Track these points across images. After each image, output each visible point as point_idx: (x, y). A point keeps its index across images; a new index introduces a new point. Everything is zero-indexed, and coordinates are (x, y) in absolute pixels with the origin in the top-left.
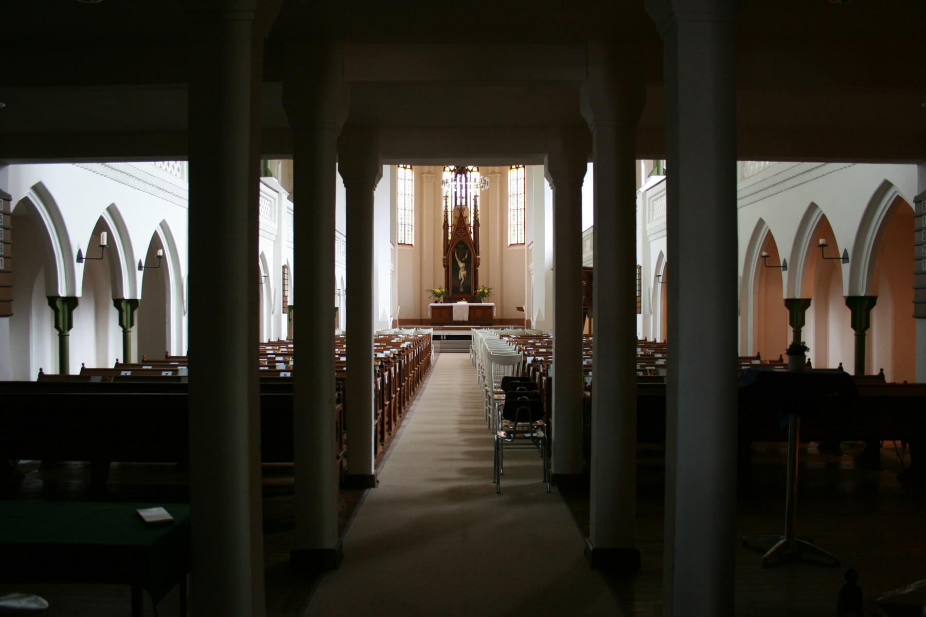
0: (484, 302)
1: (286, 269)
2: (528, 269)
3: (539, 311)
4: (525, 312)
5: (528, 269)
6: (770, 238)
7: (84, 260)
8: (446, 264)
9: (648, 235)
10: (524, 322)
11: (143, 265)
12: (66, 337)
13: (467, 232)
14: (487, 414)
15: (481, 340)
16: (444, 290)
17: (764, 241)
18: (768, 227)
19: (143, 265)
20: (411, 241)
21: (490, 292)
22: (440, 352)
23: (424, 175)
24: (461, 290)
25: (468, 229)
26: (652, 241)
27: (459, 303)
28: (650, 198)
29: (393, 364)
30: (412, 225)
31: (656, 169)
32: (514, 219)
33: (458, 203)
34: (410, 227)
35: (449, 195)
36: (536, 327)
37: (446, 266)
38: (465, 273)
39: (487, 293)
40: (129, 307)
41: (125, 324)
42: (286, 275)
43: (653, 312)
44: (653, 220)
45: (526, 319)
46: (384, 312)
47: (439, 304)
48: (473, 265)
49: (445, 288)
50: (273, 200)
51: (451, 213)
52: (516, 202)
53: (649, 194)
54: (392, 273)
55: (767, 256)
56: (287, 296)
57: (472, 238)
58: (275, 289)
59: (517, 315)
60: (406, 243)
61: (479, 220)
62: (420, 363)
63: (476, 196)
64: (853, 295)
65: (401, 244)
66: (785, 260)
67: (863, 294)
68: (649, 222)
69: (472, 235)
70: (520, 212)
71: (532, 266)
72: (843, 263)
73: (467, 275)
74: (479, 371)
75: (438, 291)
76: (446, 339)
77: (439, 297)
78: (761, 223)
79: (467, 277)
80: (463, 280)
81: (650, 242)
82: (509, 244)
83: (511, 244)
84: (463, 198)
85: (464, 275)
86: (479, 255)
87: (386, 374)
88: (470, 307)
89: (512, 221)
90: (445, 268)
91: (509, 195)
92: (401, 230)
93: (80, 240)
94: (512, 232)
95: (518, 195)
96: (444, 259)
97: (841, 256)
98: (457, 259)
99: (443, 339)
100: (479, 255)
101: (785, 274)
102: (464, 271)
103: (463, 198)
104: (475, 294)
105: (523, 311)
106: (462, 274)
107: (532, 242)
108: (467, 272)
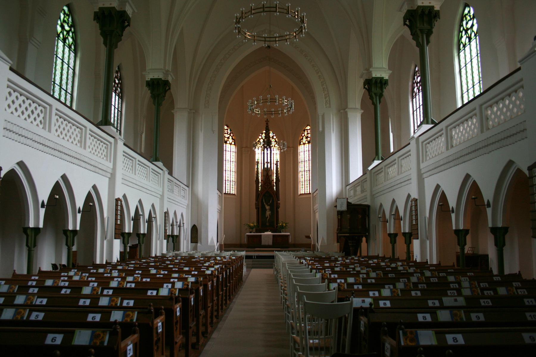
0: (283, 232)
1: (166, 214)
2: (313, 209)
3: (323, 238)
4: (312, 239)
5: (313, 209)
6: (443, 195)
7: (81, 212)
8: (257, 207)
9: (422, 172)
10: (311, 246)
11: (81, 210)
12: (71, 250)
13: (271, 185)
14: (286, 320)
15: (284, 265)
16: (255, 224)
17: (511, 182)
18: (442, 189)
19: (81, 210)
21: (287, 226)
22: (252, 268)
23: (244, 149)
24: (267, 224)
26: (425, 178)
27: (266, 233)
28: (423, 142)
29: (225, 270)
30: (235, 182)
31: (377, 156)
32: (302, 178)
33: (266, 166)
34: (234, 182)
35: (260, 161)
36: (320, 250)
37: (257, 208)
39: (285, 226)
40: (72, 235)
41: (69, 244)
42: (166, 217)
43: (429, 237)
44: (426, 160)
45: (312, 243)
46: (212, 239)
47: (252, 234)
48: (275, 208)
49: (257, 223)
50: (109, 144)
51: (260, 174)
52: (303, 166)
53: (422, 139)
54: (219, 212)
55: (476, 198)
56: (167, 230)
57: (275, 189)
58: (108, 218)
59: (305, 241)
60: (231, 193)
61: (279, 178)
62: (239, 274)
63: (277, 162)
64: (457, 229)
65: (228, 194)
66: (488, 200)
67: (500, 226)
68: (423, 162)
69: (275, 187)
70: (307, 173)
71: (317, 206)
72: (487, 207)
73: (271, 214)
74: (282, 286)
75: (252, 225)
76: (256, 258)
77: (252, 229)
78: (438, 187)
79: (272, 215)
81: (424, 179)
82: (299, 193)
83: (301, 194)
84: (269, 163)
85: (269, 214)
87: (228, 271)
88: (273, 236)
89: (301, 179)
90: (256, 209)
91: (299, 161)
92: (228, 185)
93: (44, 195)
95: (305, 162)
96: (256, 203)
97: (486, 204)
98: (265, 204)
99: (254, 258)
100: (279, 201)
102: (269, 211)
103: (269, 163)
104: (277, 227)
105: (310, 238)
106: (268, 213)
107: (317, 190)
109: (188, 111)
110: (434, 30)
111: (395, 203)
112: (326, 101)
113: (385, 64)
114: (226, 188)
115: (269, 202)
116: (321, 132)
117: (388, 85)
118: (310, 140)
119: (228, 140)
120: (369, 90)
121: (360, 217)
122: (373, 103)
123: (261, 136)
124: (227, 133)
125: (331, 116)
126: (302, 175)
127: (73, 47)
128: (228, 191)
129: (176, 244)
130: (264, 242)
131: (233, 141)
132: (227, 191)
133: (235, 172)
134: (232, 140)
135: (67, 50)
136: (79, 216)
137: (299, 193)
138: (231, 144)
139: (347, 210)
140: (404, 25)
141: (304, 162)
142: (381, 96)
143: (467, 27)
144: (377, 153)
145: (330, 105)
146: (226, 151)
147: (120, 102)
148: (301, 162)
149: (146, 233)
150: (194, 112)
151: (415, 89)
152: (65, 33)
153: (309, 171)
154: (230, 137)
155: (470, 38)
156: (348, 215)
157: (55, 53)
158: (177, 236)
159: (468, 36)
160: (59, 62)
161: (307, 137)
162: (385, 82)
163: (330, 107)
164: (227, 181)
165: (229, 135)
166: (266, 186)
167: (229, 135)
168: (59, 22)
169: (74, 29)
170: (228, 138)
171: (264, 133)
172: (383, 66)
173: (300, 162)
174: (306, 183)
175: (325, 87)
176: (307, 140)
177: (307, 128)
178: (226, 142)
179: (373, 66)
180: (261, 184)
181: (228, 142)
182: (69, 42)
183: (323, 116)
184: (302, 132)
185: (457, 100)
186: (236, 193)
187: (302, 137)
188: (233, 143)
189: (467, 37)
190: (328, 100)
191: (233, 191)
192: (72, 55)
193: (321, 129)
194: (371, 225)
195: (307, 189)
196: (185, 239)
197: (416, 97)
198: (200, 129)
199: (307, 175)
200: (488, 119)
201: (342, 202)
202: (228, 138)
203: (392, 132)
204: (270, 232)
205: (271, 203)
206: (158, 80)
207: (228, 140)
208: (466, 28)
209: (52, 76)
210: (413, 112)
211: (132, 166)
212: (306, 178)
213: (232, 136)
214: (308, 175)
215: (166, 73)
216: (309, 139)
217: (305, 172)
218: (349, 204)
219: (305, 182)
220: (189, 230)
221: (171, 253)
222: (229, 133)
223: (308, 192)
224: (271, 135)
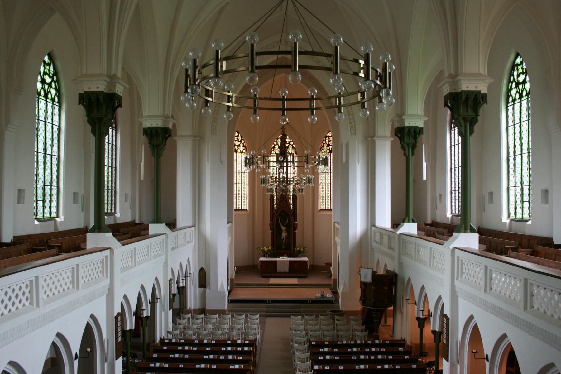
3: (345, 284)
16: (270, 248)
20: (246, 207)
21: (305, 250)
22: (267, 316)
24: (283, 247)
25: (289, 201)
30: (247, 195)
32: (323, 191)
34: (246, 196)
37: (272, 229)
38: (286, 234)
39: (303, 251)
46: (222, 284)
48: (292, 228)
49: (272, 245)
52: (324, 178)
58: (108, 340)
60: (243, 208)
65: (239, 210)
69: (292, 206)
70: (328, 186)
78: (471, 318)
80: (285, 240)
82: (319, 209)
83: (321, 210)
85: (285, 236)
86: (297, 221)
88: (290, 262)
89: (321, 192)
90: (271, 231)
92: (239, 199)
94: (321, 201)
96: (270, 224)
98: (280, 224)
100: (297, 221)
101: (487, 364)
102: (285, 233)
104: (294, 250)
106: (284, 234)
108: (288, 234)
109: (193, 139)
110: (479, 118)
111: (424, 291)
112: (351, 128)
113: (420, 111)
114: (237, 203)
115: (286, 223)
116: (344, 163)
117: (423, 134)
118: (332, 149)
119: (239, 149)
120: (401, 139)
121: (386, 289)
122: (405, 154)
123: (276, 141)
124: (237, 140)
125: (357, 144)
126: (323, 188)
127: (56, 99)
128: (239, 206)
129: (182, 296)
130: (279, 269)
131: (244, 149)
132: (237, 206)
133: (247, 184)
134: (243, 148)
135: (50, 105)
136: (76, 363)
137: (319, 209)
138: (242, 152)
139: (371, 282)
140: (445, 107)
141: (325, 174)
142: (414, 147)
143: (518, 80)
144: (407, 214)
145: (355, 131)
146: (236, 161)
147: (114, 134)
148: (321, 173)
149: (149, 315)
150: (199, 139)
151: (513, 92)
152: (46, 86)
153: (331, 184)
154: (241, 145)
155: (521, 96)
156: (373, 287)
157: (36, 151)
158: (183, 287)
159: (518, 90)
160: (42, 124)
161: (328, 146)
162: (420, 130)
163: (355, 134)
164: (237, 196)
165: (240, 142)
166: (281, 204)
167: (240, 142)
168: (39, 78)
169: (57, 78)
170: (239, 146)
171: (280, 138)
172: (417, 112)
173: (320, 173)
174: (326, 198)
175: (350, 111)
176: (329, 148)
177: (328, 135)
178: (236, 151)
179: (407, 113)
180: (276, 197)
181: (239, 151)
182: (51, 96)
183: (347, 144)
184: (323, 139)
185: (501, 162)
186: (248, 209)
187: (323, 144)
188: (244, 151)
189: (517, 92)
190: (353, 126)
191: (246, 206)
192: (56, 108)
193: (344, 160)
194: (398, 296)
195: (328, 205)
196: (192, 284)
197: (454, 130)
198: (206, 159)
199: (328, 188)
200: (533, 296)
201: (366, 273)
202: (239, 146)
203: (425, 162)
204: (286, 257)
205: (288, 223)
206: (157, 129)
207: (239, 149)
208: (517, 80)
209: (35, 139)
210: (451, 169)
211: (131, 257)
212: (326, 192)
213: (243, 144)
214: (329, 189)
215: (166, 117)
216: (331, 147)
217: (326, 185)
218: (374, 274)
219: (325, 197)
220: (196, 279)
221: (177, 331)
222: (239, 140)
223: (329, 209)
224: (288, 140)
